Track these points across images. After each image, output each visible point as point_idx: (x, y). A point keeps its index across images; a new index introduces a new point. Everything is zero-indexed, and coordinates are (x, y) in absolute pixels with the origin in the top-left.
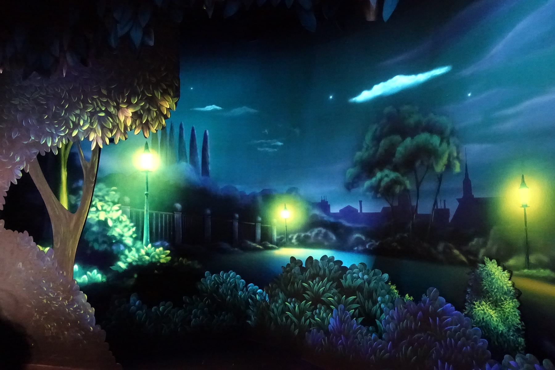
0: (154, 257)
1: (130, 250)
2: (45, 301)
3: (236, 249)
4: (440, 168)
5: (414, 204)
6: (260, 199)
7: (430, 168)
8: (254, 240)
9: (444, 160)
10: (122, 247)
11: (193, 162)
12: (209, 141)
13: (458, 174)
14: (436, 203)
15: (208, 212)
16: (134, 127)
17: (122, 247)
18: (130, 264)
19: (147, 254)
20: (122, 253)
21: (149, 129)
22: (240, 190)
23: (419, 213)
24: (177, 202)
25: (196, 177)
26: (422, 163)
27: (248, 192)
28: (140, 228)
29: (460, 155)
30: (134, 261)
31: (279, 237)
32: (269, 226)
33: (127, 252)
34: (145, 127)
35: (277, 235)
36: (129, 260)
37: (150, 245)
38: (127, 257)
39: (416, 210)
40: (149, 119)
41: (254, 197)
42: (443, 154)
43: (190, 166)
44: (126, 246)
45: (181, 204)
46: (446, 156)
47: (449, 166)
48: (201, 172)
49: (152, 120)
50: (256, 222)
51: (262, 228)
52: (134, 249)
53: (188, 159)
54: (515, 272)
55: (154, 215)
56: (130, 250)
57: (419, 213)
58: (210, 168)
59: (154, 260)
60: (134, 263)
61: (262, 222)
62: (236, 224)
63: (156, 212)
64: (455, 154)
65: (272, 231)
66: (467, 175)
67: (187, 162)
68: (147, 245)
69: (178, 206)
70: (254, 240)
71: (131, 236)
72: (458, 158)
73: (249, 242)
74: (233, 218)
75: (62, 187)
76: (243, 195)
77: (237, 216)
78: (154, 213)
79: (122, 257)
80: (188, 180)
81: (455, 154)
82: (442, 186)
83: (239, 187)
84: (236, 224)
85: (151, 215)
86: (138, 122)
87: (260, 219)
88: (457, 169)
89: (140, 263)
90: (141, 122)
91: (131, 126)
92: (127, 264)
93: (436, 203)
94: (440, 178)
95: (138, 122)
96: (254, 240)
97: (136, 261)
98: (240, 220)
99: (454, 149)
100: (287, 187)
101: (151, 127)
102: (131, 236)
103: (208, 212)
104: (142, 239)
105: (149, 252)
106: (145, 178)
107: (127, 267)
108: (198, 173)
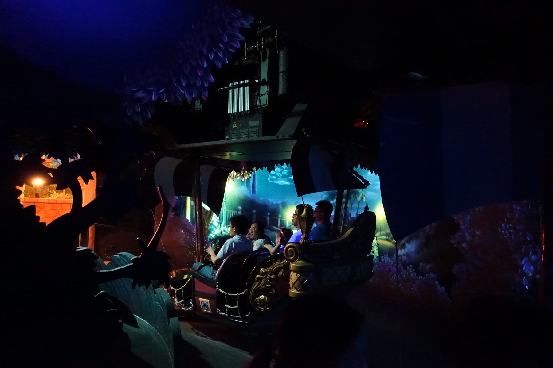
0: (227, 232)
1: (216, 228)
2: (194, 247)
3: (268, 230)
4: (359, 199)
5: (349, 212)
6: (280, 206)
7: (356, 198)
8: (277, 226)
9: (361, 196)
10: (213, 227)
11: (248, 187)
12: (256, 176)
13: (365, 202)
14: (357, 212)
15: (255, 211)
16: (237, 176)
17: (213, 227)
18: (216, 235)
19: (224, 231)
20: (213, 230)
21: (244, 177)
22: (271, 201)
23: (351, 216)
24: (239, 206)
25: (249, 194)
26: (353, 196)
27: (275, 203)
28: (221, 219)
29: (366, 195)
30: (218, 234)
31: (289, 225)
32: (284, 219)
33: (214, 229)
34: (242, 177)
35: (289, 224)
36: (216, 233)
37: (225, 226)
38: (214, 232)
39: (350, 215)
40: (244, 174)
41: (277, 205)
42: (360, 194)
43: (246, 188)
44: (214, 226)
45: (241, 207)
46: (361, 195)
47: (362, 199)
48: (251, 191)
49: (245, 174)
50: (278, 217)
51: (281, 221)
52: (218, 228)
53: (246, 186)
54: (378, 238)
55: (228, 212)
56: (216, 228)
57: (351, 216)
58: (256, 190)
59: (227, 234)
60: (218, 235)
61: (281, 218)
62: (268, 218)
63: (229, 210)
64: (364, 195)
65: (286, 221)
66: (367, 203)
67: (245, 186)
68: (224, 227)
69: (240, 208)
70: (277, 226)
71: (217, 222)
72: (365, 196)
73: (274, 227)
74: (267, 215)
75: (285, 210)
76: (272, 204)
77: (269, 214)
78: (228, 211)
79: (212, 232)
80: (245, 195)
81: (364, 195)
82: (359, 206)
83: (271, 200)
84: (268, 218)
85: (226, 212)
86: (239, 174)
87: (280, 216)
88: (364, 200)
89: (220, 235)
90: (241, 174)
91: (236, 176)
92: (214, 235)
93: (357, 212)
94: (359, 203)
95: (239, 174)
96: (277, 226)
97: (219, 234)
98: (270, 216)
99: (364, 192)
100: (295, 201)
101: (245, 177)
102: (217, 222)
103: (255, 211)
104: (222, 223)
105: (225, 230)
106: (380, 227)
107: (215, 237)
108: (250, 192)
